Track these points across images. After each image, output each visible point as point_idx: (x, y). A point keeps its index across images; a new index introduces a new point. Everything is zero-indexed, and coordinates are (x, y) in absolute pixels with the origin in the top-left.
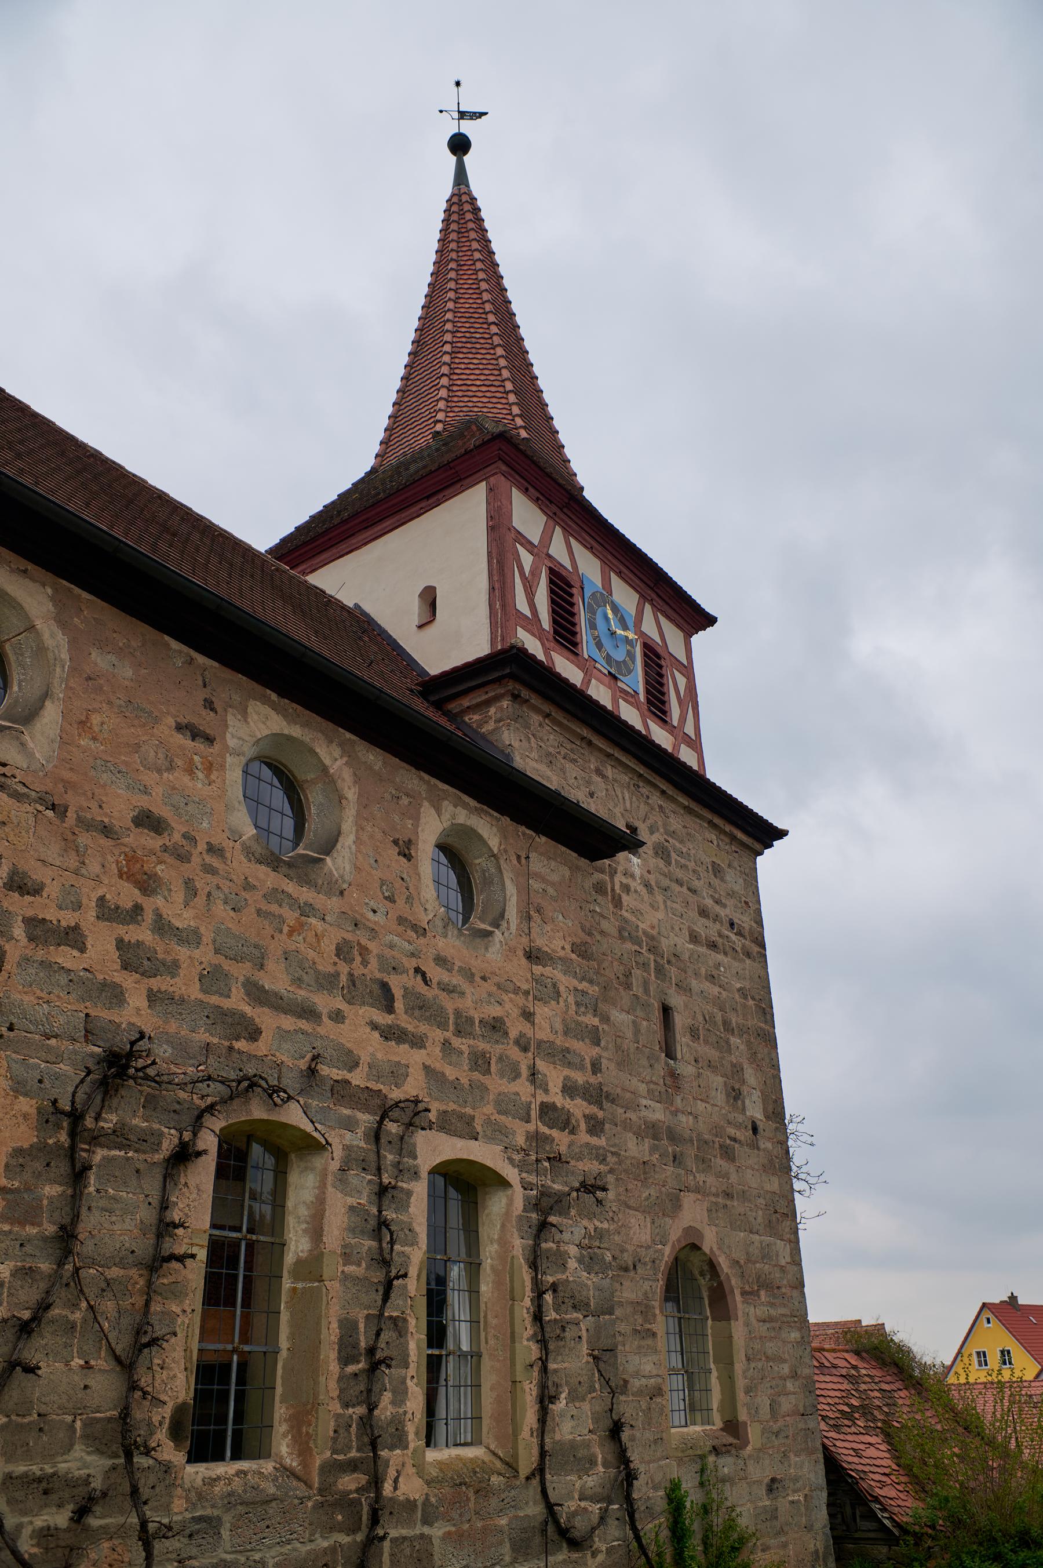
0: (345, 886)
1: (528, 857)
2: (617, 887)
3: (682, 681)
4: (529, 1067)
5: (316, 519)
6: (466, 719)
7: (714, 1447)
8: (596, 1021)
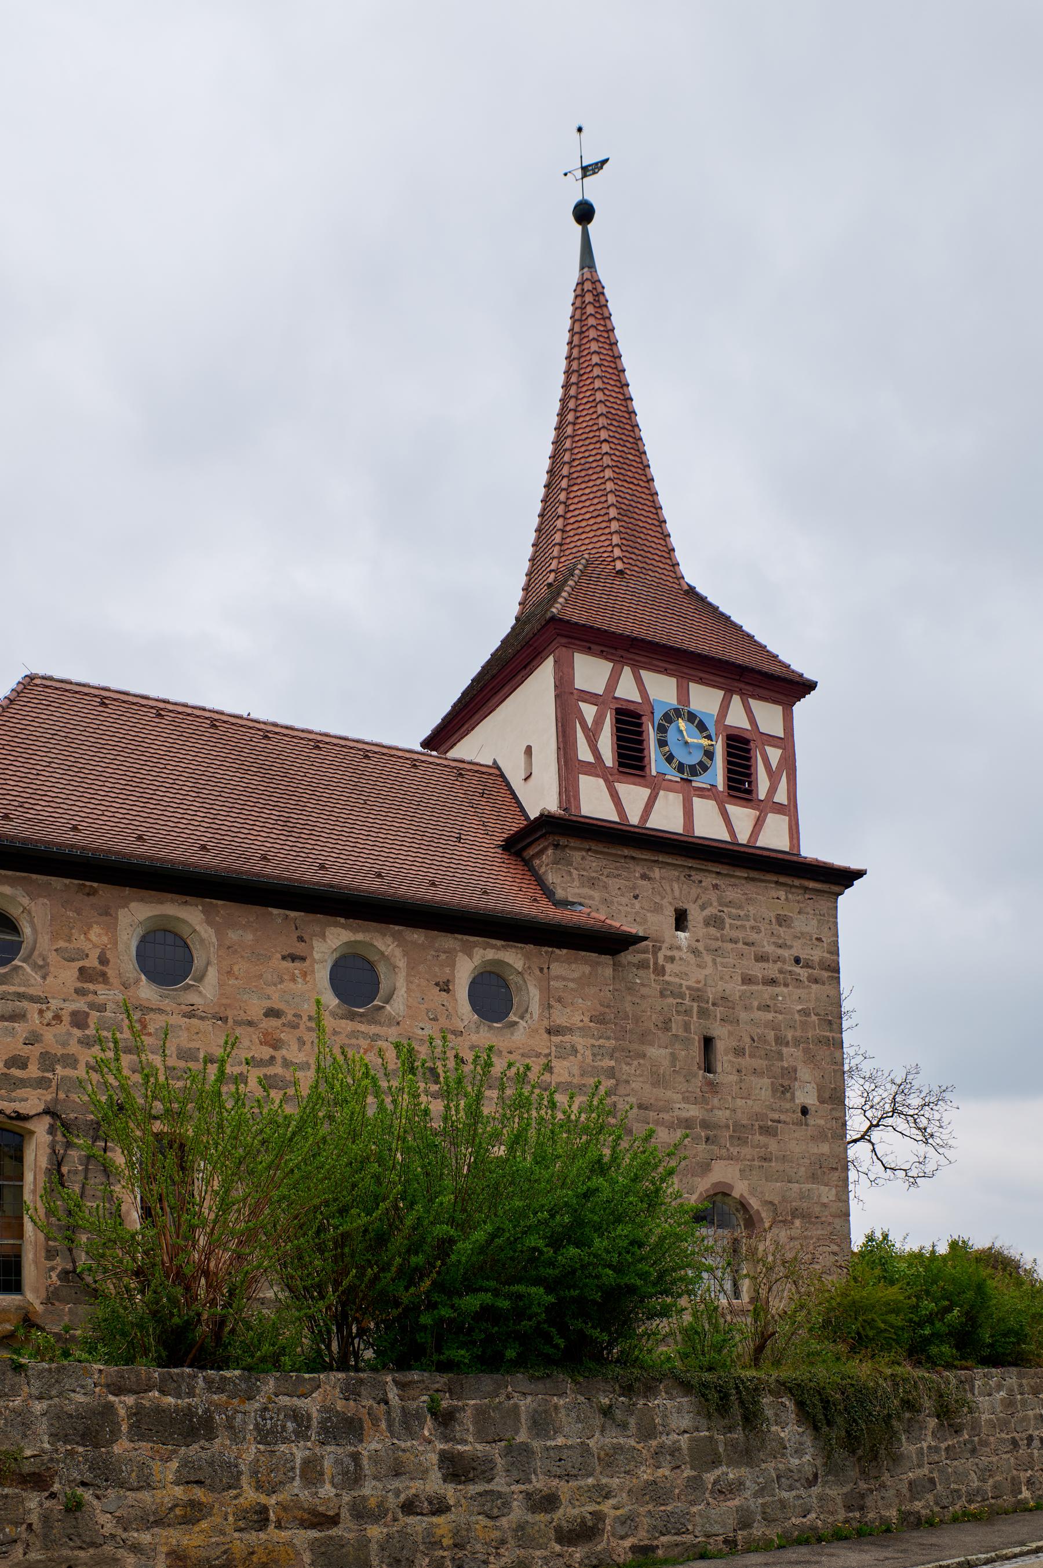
0: (400, 1019)
1: (548, 968)
5: (460, 700)
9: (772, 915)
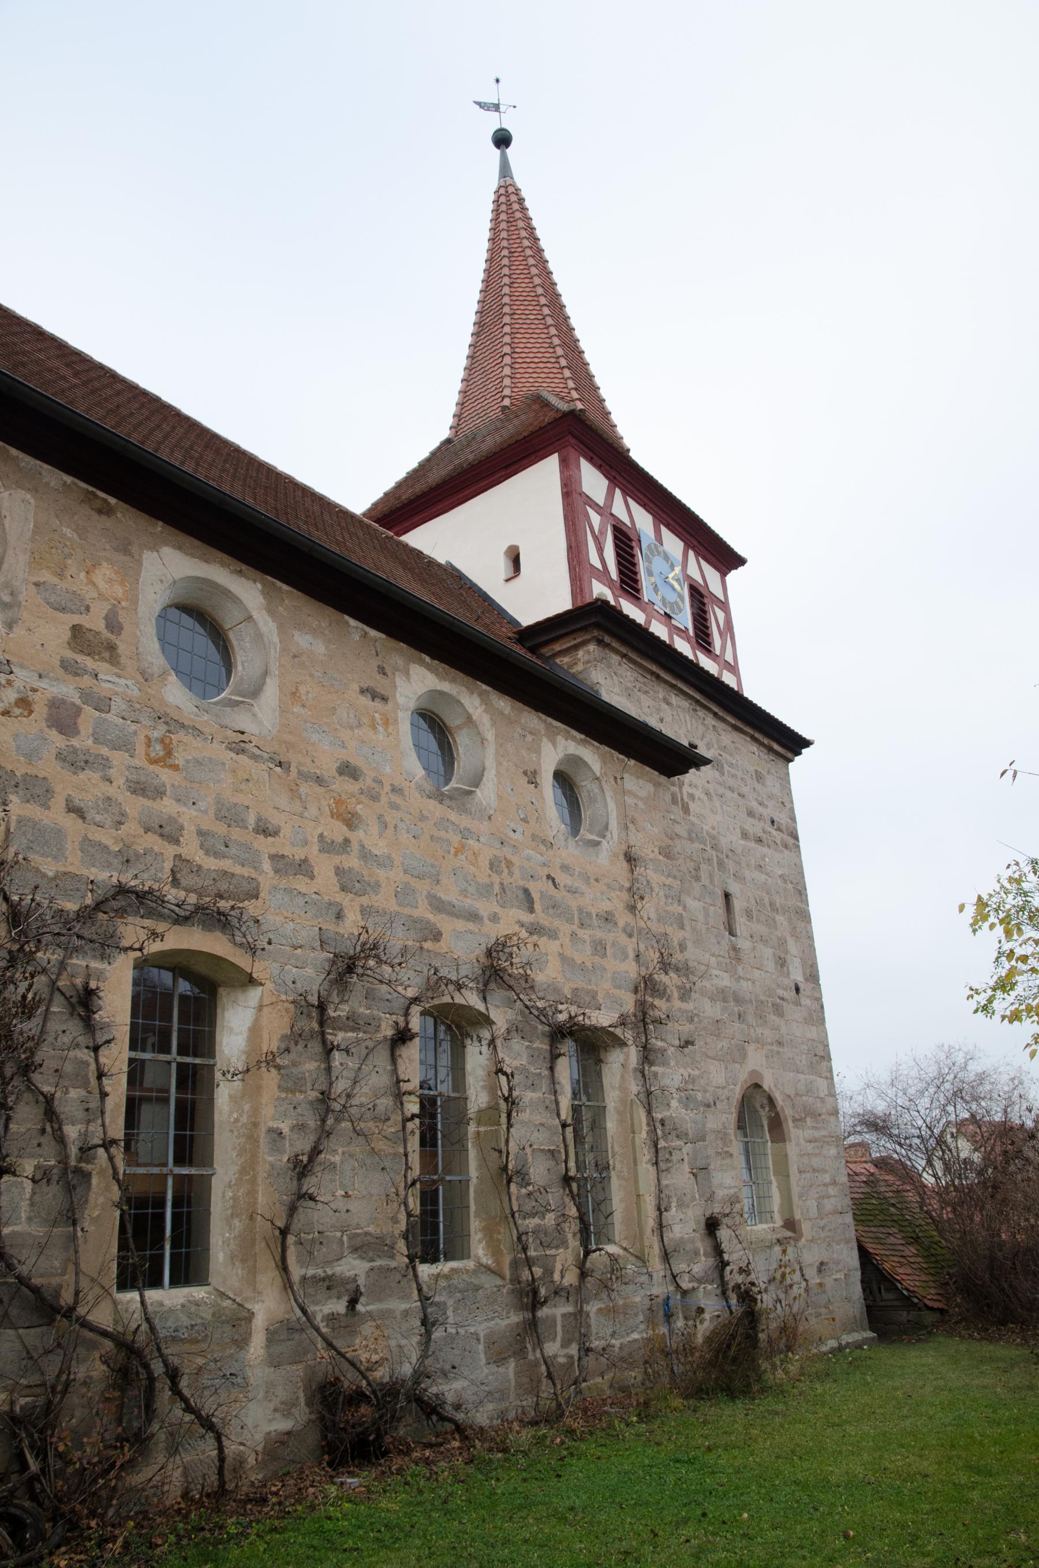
0: (492, 812)
2: (685, 797)
3: (721, 615)
4: (634, 950)
6: (558, 661)
7: (778, 1240)
8: (680, 909)
9: (752, 769)
